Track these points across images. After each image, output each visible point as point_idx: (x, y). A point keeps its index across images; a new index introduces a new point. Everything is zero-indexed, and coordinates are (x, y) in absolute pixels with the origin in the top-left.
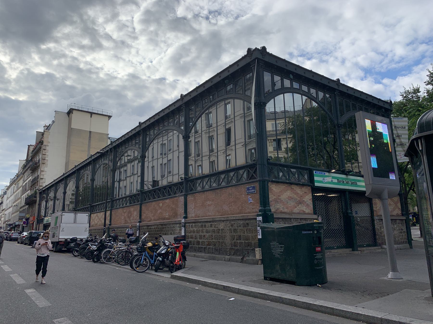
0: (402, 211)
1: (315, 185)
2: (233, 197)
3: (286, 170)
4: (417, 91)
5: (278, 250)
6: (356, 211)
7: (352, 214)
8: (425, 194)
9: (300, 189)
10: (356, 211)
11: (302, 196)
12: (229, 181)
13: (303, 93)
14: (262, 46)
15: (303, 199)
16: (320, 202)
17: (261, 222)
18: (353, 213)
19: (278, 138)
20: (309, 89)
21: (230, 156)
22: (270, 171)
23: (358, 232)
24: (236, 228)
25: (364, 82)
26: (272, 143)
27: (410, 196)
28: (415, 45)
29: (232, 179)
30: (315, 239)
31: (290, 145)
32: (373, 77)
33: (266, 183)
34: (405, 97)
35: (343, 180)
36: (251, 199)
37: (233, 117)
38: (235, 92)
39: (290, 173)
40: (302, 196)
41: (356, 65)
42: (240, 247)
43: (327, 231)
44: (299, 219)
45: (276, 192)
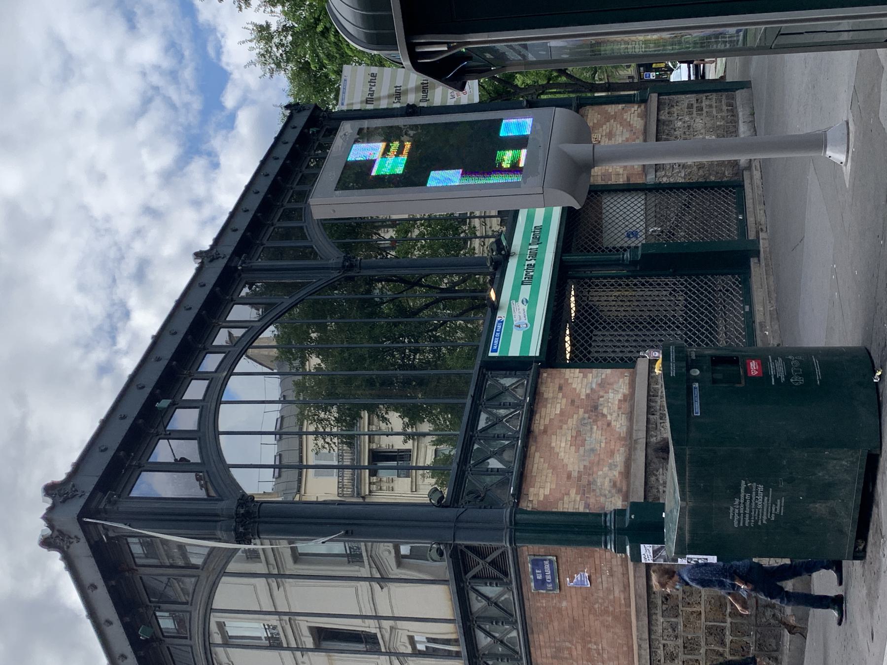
0: (629, 100)
1: (538, 354)
2: (568, 644)
3: (480, 444)
4: (263, 32)
5: (760, 502)
6: (628, 236)
7: (636, 247)
8: (581, 46)
9: (549, 405)
10: (628, 236)
11: (573, 402)
12: (510, 653)
13: (228, 369)
14: (39, 492)
15: (583, 397)
16: (593, 344)
17: (659, 550)
18: (633, 245)
19: (366, 464)
20: (217, 350)
21: (417, 638)
22: (482, 500)
23: (695, 234)
24: (680, 642)
25: (223, 160)
26: (384, 479)
27: (587, 72)
28: (139, 11)
29: (502, 642)
30: (719, 376)
31: (396, 421)
32: (211, 132)
33: (525, 516)
34: (278, 65)
35: (526, 268)
36: (577, 577)
37: (277, 617)
38: (186, 603)
39: (492, 432)
40: (573, 402)
41: (168, 177)
42: (749, 635)
43: (690, 330)
44: (651, 417)
45: (554, 486)
